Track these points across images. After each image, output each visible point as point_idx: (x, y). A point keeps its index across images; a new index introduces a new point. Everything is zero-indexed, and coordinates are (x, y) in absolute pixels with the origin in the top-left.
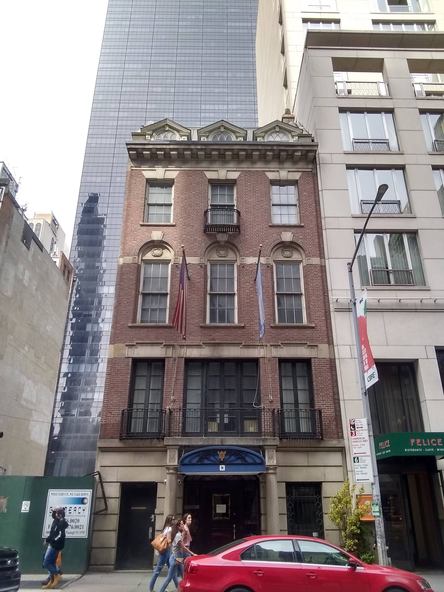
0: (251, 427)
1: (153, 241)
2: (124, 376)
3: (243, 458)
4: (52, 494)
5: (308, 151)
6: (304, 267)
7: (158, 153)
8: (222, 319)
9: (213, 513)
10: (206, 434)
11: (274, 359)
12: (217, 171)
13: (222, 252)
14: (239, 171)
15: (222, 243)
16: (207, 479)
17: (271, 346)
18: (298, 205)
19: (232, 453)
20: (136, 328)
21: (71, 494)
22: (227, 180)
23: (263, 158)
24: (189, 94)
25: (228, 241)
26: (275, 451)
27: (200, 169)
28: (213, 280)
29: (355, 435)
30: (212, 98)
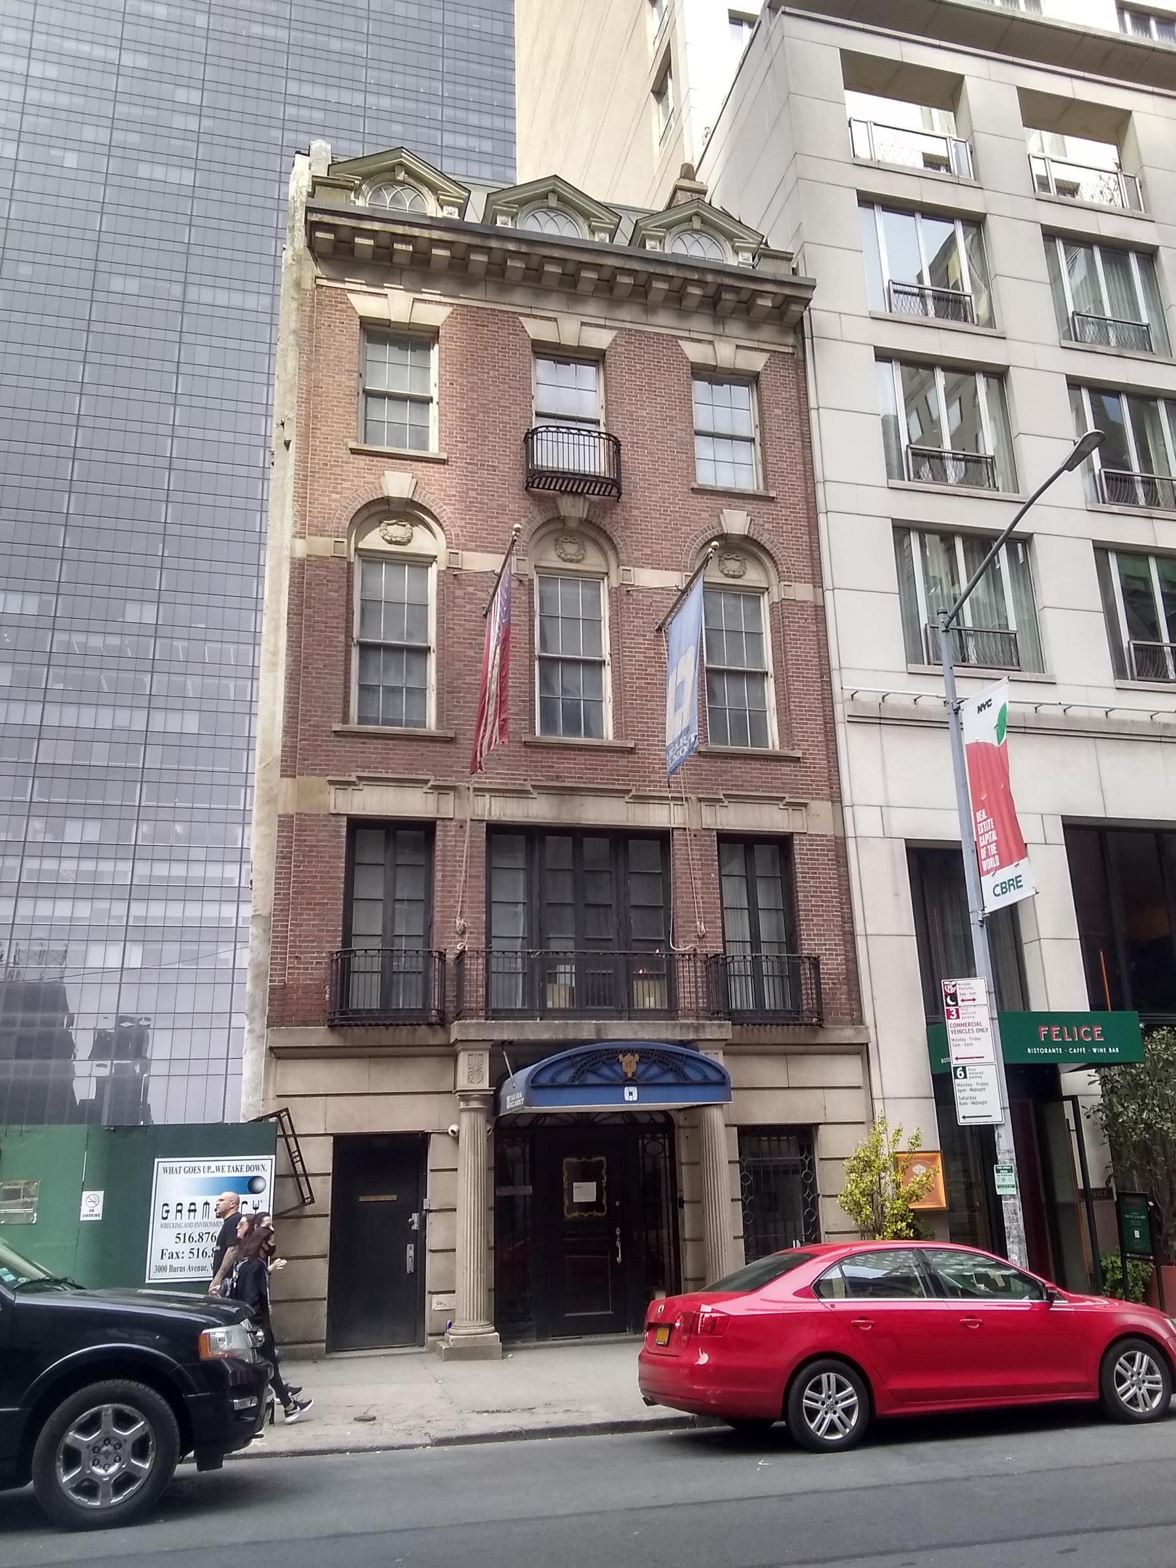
0: (649, 997)
1: (387, 500)
2: (328, 862)
3: (678, 1071)
4: (165, 1170)
5: (789, 300)
6: (772, 606)
7: (397, 246)
8: (572, 726)
9: (567, 1203)
10: (546, 1013)
11: (707, 833)
12: (555, 320)
13: (571, 549)
14: (611, 328)
15: (572, 524)
16: (548, 1121)
17: (700, 800)
18: (758, 440)
19: (654, 1058)
20: (354, 737)
21: (218, 1169)
22: (410, 326)
23: (676, 301)
24: (252, 42)
25: (586, 520)
26: (721, 1053)
27: (509, 308)
28: (547, 622)
29: (958, 1017)
30: (321, 67)
